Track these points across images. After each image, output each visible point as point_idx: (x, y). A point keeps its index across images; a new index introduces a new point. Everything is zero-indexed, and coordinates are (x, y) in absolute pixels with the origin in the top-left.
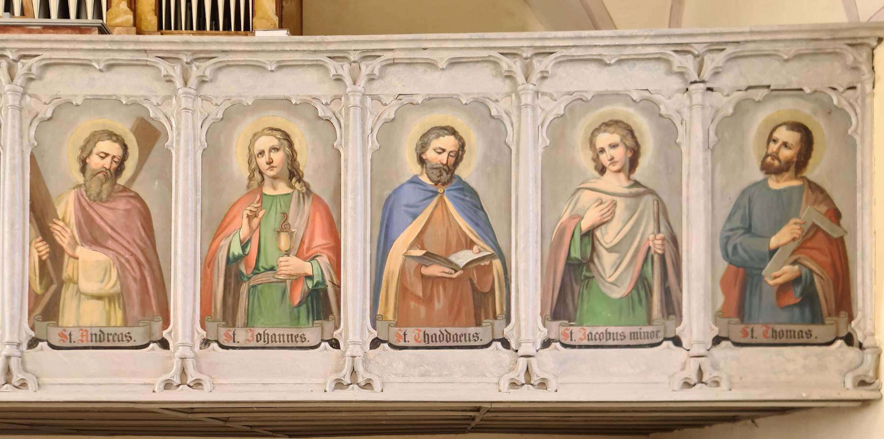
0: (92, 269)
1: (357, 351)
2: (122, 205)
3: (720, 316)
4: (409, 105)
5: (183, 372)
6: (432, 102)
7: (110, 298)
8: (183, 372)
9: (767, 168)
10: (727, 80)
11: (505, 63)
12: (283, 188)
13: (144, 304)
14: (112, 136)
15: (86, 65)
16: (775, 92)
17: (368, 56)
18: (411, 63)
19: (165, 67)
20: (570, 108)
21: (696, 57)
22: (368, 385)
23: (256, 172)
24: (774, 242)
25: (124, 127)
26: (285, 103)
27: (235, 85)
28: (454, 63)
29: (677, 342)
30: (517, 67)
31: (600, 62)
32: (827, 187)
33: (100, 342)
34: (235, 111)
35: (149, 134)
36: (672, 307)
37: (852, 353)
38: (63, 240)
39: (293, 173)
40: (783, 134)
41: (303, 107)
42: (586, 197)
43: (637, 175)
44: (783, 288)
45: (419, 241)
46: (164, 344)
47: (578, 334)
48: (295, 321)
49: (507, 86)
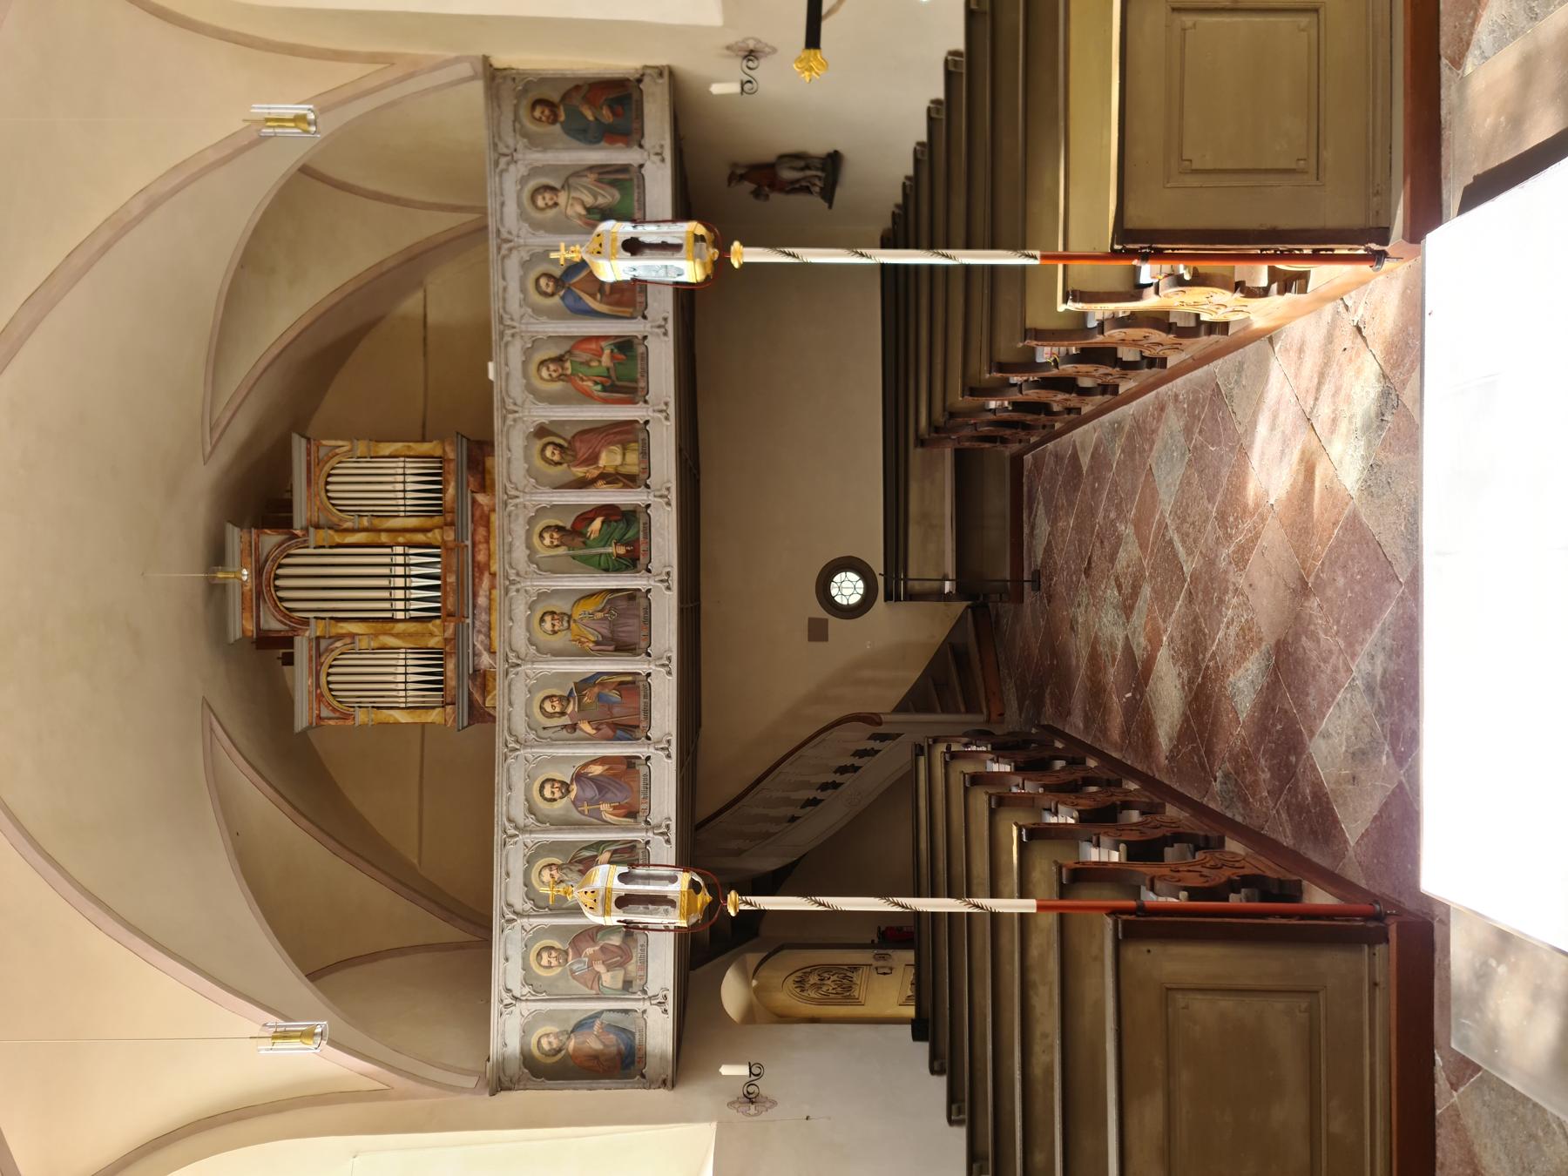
0: (609, 459)
1: (648, 327)
2: (578, 444)
3: (628, 145)
4: (525, 301)
5: (662, 834)
6: (523, 290)
7: (624, 449)
8: (662, 834)
9: (554, 121)
10: (511, 142)
11: (503, 252)
12: (568, 365)
13: (627, 432)
14: (543, 450)
15: (509, 461)
16: (516, 119)
17: (501, 319)
18: (504, 300)
19: (509, 422)
20: (526, 220)
21: (502, 157)
22: (665, 319)
23: (559, 378)
24: (591, 118)
25: (539, 444)
26: (525, 363)
27: (517, 388)
28: (504, 278)
29: (641, 166)
30: (506, 246)
31: (503, 204)
32: (563, 91)
33: (645, 453)
34: (530, 388)
35: (542, 431)
36: (625, 169)
37: (646, 80)
38: (596, 473)
39: (559, 360)
40: (537, 114)
41: (528, 353)
42: (570, 212)
43: (558, 186)
44: (614, 113)
45: (593, 296)
46: (647, 422)
47: (643, 724)
48: (634, 358)
49: (515, 252)
